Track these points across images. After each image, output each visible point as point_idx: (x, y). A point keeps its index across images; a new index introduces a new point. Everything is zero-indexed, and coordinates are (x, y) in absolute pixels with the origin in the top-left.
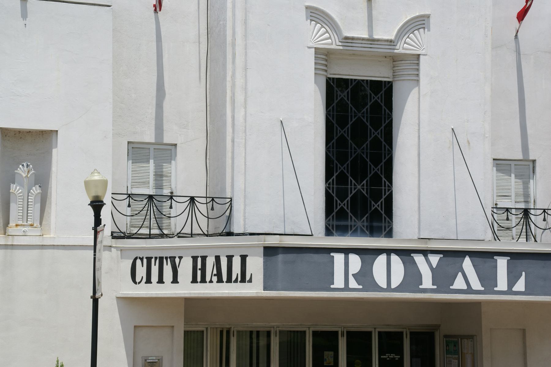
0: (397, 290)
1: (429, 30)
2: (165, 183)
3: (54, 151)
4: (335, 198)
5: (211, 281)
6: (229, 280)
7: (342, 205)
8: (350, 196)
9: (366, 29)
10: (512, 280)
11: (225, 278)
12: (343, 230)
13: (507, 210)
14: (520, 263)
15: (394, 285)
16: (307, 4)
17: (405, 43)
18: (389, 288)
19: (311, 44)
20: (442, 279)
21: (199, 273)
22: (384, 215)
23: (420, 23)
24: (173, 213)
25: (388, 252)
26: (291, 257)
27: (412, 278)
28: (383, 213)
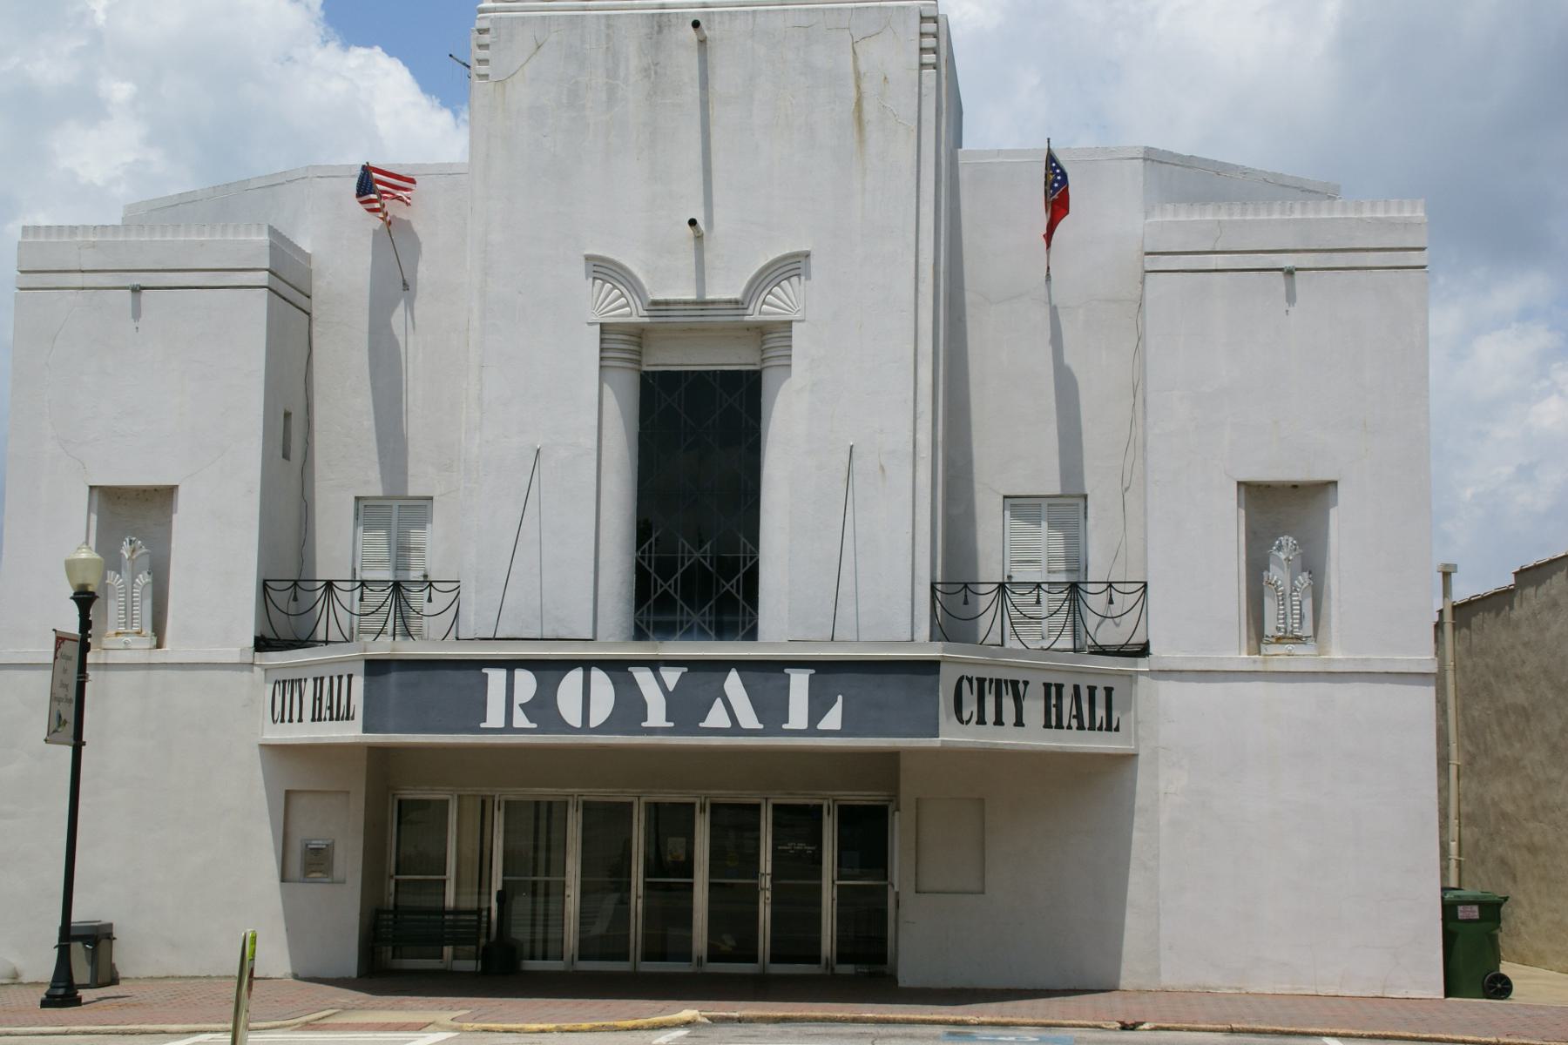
0: (599, 730)
1: (808, 278)
2: (413, 561)
3: (1333, 512)
4: (654, 575)
5: (1069, 727)
6: (1092, 728)
7: (666, 586)
8: (680, 571)
9: (693, 285)
10: (817, 709)
11: (1087, 724)
12: (666, 630)
13: (1038, 585)
14: (832, 678)
15: (594, 723)
16: (588, 252)
17: (764, 302)
18: (585, 728)
19: (593, 319)
20: (686, 710)
21: (1053, 710)
22: (742, 602)
23: (792, 266)
24: (428, 609)
25: (587, 665)
26: (413, 675)
27: (630, 708)
28: (740, 598)
